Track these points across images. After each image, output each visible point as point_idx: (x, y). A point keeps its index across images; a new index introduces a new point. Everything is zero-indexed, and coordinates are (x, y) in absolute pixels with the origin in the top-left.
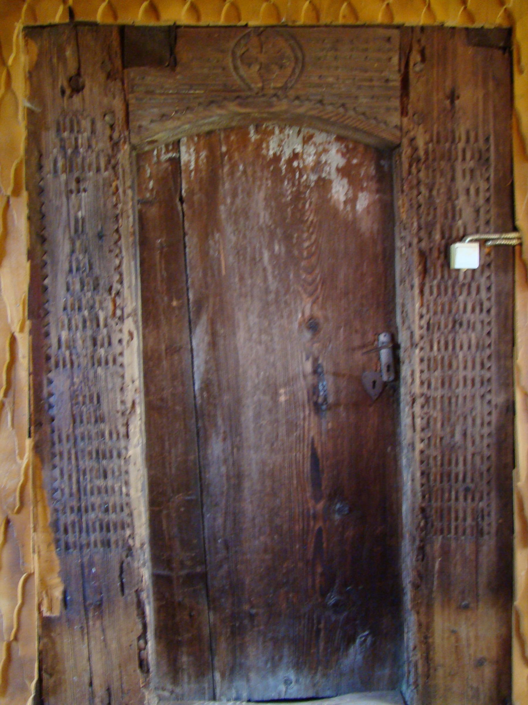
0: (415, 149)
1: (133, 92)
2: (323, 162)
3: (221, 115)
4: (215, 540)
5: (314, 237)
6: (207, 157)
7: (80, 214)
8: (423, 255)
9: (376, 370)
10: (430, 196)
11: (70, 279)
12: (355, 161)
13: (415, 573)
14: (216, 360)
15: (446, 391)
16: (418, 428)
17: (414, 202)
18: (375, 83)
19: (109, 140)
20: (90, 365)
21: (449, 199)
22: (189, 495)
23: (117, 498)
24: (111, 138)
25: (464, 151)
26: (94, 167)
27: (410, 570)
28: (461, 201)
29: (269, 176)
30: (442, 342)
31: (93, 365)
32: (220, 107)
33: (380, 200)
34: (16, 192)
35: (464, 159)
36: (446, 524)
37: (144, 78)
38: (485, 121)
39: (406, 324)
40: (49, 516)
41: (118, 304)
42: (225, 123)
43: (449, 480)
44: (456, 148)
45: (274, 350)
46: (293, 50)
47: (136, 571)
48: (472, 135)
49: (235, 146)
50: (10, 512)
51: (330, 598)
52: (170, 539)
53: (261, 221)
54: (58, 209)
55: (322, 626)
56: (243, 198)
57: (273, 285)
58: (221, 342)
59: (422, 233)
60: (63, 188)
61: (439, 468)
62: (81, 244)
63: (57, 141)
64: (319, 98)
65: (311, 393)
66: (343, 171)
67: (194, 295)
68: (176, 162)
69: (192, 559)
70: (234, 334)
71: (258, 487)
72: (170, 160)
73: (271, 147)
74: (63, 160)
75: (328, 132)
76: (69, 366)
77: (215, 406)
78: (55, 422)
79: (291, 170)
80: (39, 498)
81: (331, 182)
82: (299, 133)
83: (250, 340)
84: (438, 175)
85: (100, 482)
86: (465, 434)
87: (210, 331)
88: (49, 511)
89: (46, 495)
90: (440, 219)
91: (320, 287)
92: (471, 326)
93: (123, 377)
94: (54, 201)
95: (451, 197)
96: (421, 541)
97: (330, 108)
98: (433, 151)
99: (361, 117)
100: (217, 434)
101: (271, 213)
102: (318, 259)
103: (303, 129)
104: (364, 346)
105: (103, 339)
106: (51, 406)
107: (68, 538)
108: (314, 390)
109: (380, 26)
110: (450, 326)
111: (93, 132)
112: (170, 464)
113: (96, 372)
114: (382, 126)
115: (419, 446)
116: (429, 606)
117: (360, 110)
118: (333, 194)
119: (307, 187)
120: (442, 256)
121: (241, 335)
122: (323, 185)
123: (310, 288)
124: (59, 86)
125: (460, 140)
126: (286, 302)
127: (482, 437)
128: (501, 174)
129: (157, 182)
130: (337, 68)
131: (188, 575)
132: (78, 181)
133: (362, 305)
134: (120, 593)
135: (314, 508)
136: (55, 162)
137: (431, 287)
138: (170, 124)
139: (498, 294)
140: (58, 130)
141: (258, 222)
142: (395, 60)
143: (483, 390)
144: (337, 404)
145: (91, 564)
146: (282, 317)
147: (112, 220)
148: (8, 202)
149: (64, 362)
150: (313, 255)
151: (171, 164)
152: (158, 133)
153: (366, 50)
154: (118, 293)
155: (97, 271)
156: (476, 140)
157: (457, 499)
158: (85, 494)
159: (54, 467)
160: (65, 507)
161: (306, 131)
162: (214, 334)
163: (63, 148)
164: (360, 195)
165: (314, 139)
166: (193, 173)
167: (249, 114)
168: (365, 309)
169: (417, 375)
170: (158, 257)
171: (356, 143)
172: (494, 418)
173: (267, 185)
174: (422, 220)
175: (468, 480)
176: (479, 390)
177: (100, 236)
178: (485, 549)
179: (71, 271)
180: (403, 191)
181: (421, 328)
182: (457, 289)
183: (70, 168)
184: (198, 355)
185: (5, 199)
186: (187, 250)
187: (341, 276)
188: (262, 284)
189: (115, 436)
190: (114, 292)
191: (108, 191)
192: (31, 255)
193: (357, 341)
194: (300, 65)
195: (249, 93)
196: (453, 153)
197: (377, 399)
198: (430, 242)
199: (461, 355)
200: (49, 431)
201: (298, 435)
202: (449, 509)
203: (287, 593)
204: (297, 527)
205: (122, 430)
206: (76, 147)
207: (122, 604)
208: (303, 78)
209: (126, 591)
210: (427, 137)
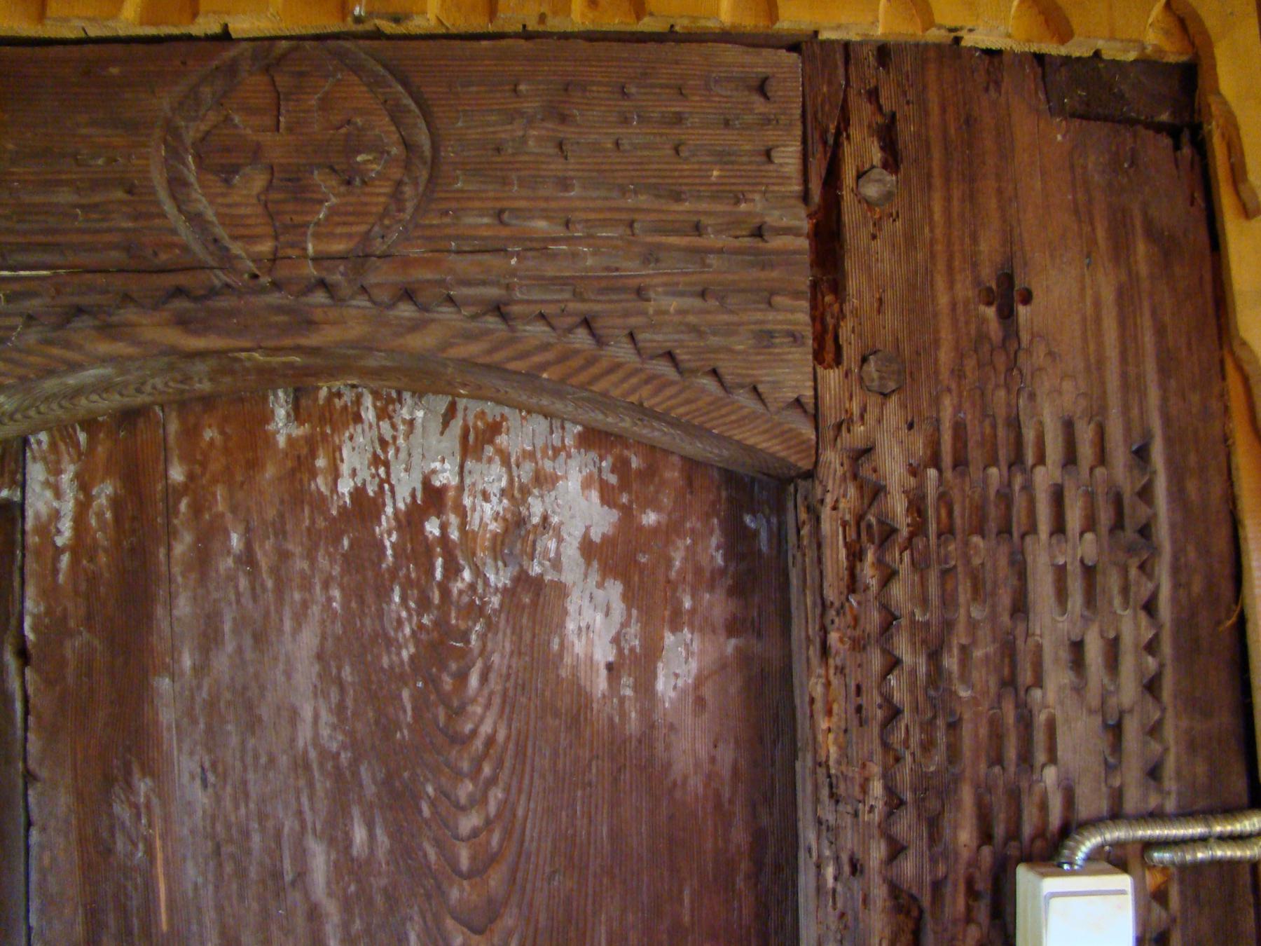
0: (876, 492)
2: (536, 520)
5: (496, 794)
6: (116, 503)
10: (936, 673)
12: (650, 518)
17: (872, 699)
18: (711, 240)
21: (1009, 683)
25: (1058, 497)
29: (336, 571)
32: (109, 330)
33: (744, 658)
35: (1059, 528)
38: (1131, 386)
44: (1028, 487)
46: (396, 115)
48: (1085, 435)
49: (216, 466)
53: (304, 734)
56: (240, 650)
59: (905, 826)
64: (493, 292)
73: (345, 469)
81: (561, 590)
90: (973, 765)
98: (944, 498)
101: (340, 709)
102: (513, 880)
103: (462, 403)
109: (726, 37)
114: (744, 399)
117: (651, 339)
119: (475, 610)
120: (983, 911)
122: (535, 603)
125: (1041, 460)
128: (1197, 587)
130: (564, 184)
141: (293, 740)
142: (788, 157)
150: (493, 859)
153: (678, 119)
156: (1102, 457)
161: (475, 407)
164: (669, 638)
165: (502, 440)
166: (65, 559)
171: (652, 450)
173: (330, 600)
174: (905, 774)
180: (825, 651)
195: (219, 278)
196: (1020, 502)
201: (766, 436)
210: (919, 446)
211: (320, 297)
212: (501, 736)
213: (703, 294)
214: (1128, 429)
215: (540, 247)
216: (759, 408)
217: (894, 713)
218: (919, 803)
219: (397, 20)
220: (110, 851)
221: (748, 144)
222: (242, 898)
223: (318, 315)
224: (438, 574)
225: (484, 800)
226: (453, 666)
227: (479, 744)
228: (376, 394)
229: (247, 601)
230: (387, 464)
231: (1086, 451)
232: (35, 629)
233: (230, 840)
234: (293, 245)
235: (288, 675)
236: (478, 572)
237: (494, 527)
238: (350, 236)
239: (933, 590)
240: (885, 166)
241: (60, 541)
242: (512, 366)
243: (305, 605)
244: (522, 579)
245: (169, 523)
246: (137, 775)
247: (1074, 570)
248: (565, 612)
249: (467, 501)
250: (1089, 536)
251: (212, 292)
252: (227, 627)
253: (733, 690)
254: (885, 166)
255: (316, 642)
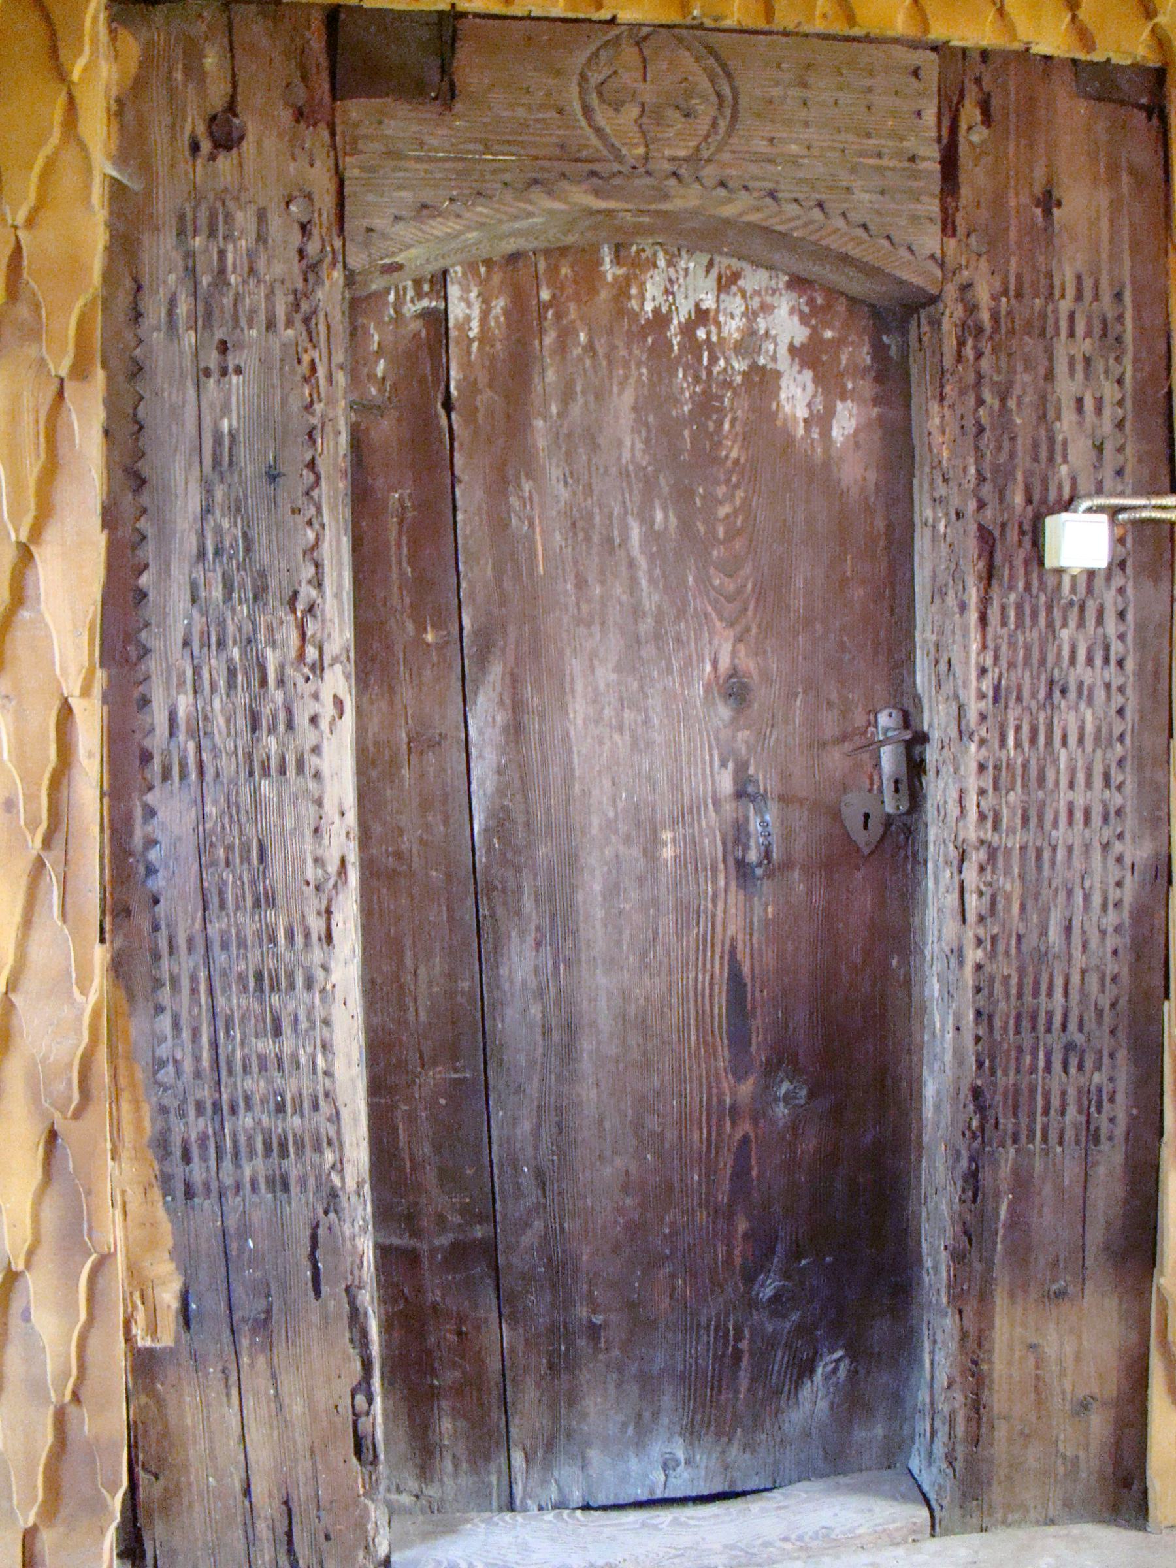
0: (972, 309)
1: (355, 152)
2: (762, 332)
3: (551, 212)
4: (516, 1168)
5: (740, 494)
6: (506, 312)
7: (225, 425)
8: (986, 537)
9: (870, 790)
11: (199, 574)
12: (828, 334)
13: (959, 1228)
14: (523, 768)
15: (1032, 837)
16: (971, 916)
17: (970, 422)
18: (885, 162)
19: (297, 258)
20: (242, 775)
22: (456, 1070)
23: (305, 1082)
24: (301, 253)
25: (1072, 317)
26: (262, 317)
27: (948, 1224)
28: (1066, 425)
29: (644, 357)
30: (1026, 729)
31: (251, 774)
34: (80, 371)
35: (1072, 334)
36: (1024, 1121)
37: (380, 123)
38: (1114, 257)
39: (948, 688)
40: (147, 1124)
41: (309, 633)
42: (554, 236)
43: (1034, 1028)
44: (1056, 311)
45: (649, 744)
47: (349, 1245)
50: (57, 1115)
51: (763, 1285)
52: (413, 1169)
53: (626, 455)
54: (176, 412)
55: (744, 1345)
56: (586, 403)
57: (650, 598)
58: (533, 725)
59: (987, 490)
60: (188, 363)
61: (1013, 999)
62: (227, 495)
63: (177, 257)
64: (770, 185)
65: (730, 840)
66: (804, 355)
67: (474, 620)
68: (437, 320)
69: (464, 1211)
70: (564, 707)
71: (613, 1050)
72: (426, 314)
73: (648, 296)
74: (191, 299)
75: (770, 267)
76: (193, 776)
77: (518, 869)
78: (161, 909)
79: (693, 346)
80: (123, 1082)
81: (778, 374)
82: (710, 265)
83: (598, 720)
84: (1020, 367)
85: (266, 1046)
86: (1068, 929)
87: (508, 701)
88: (146, 1111)
89: (140, 1076)
91: (752, 606)
92: (1085, 694)
93: (319, 803)
94: (166, 394)
95: (1044, 415)
96: (972, 1159)
97: (792, 209)
99: (860, 232)
100: (522, 933)
101: (647, 441)
103: (717, 258)
104: (844, 738)
105: (275, 717)
106: (151, 871)
107: (191, 1172)
108: (738, 834)
109: (896, 41)
110: (1042, 695)
111: (261, 238)
112: (415, 1000)
113: (256, 790)
114: (903, 252)
115: (974, 956)
116: (985, 1297)
118: (784, 402)
119: (727, 384)
121: (579, 709)
122: (761, 382)
123: (730, 608)
124: (187, 134)
125: (1063, 296)
126: (678, 640)
127: (1103, 933)
129: (392, 362)
131: (454, 1245)
132: (223, 347)
133: (842, 646)
134: (312, 1294)
135: (733, 1094)
136: (172, 303)
137: (1003, 608)
138: (438, 227)
139: (1141, 627)
140: (181, 233)
141: (619, 458)
143: (1107, 833)
144: (787, 865)
145: (245, 1231)
146: (669, 670)
147: (300, 440)
148: (60, 394)
149: (183, 766)
150: (739, 532)
151: (426, 325)
152: (409, 247)
153: (870, 90)
154: (311, 609)
155: (263, 556)
156: (1096, 297)
157: (1048, 1069)
158: (230, 1072)
159: (159, 1009)
160: (184, 1101)
161: (725, 261)
162: (517, 707)
163: (191, 272)
164: (839, 406)
165: (741, 282)
166: (475, 345)
167: (609, 213)
168: (848, 656)
169: (972, 799)
170: (393, 535)
171: (832, 293)
172: (1128, 894)
175: (1073, 1026)
176: (1100, 833)
177: (273, 476)
178: (1101, 1170)
179: (202, 555)
181: (982, 696)
182: (1057, 615)
183: (205, 318)
184: (481, 756)
185: (54, 387)
186: (460, 517)
187: (799, 583)
188: (624, 598)
189: (299, 939)
190: (301, 606)
191: (293, 372)
192: (110, 518)
193: (830, 725)
194: (728, 112)
195: (616, 167)
196: (1050, 322)
197: (872, 853)
198: (1002, 511)
199: (1063, 755)
200: (146, 927)
202: (1033, 1090)
203: (673, 1276)
204: (696, 1136)
205: (317, 925)
206: (222, 271)
207: (316, 1318)
208: (734, 140)
209: (325, 1289)
211: (673, 182)
212: (742, 460)
213: (882, 193)
214: (1111, 284)
215: (794, 160)
216: (911, 257)
217: (981, 430)
218: (994, 480)
219: (716, 20)
220: (507, 525)
221: (906, 107)
222: (589, 554)
223: (673, 192)
224: (705, 362)
225: (733, 496)
226: (715, 417)
227: (729, 463)
228: (666, 252)
229: (590, 373)
230: (673, 294)
231: (1088, 294)
232: (457, 388)
233: (582, 518)
234: (658, 151)
235: (617, 418)
236: (727, 360)
237: (736, 336)
238: (688, 147)
239: (1003, 364)
240: (983, 123)
241: (472, 334)
242: (778, 228)
243: (626, 377)
244: (754, 367)
245: (540, 324)
246: (523, 479)
247: (1079, 357)
248: (780, 388)
249: (722, 319)
250: (1088, 341)
251: (614, 175)
252: (579, 388)
253: (876, 437)
254: (983, 123)
255: (632, 400)
